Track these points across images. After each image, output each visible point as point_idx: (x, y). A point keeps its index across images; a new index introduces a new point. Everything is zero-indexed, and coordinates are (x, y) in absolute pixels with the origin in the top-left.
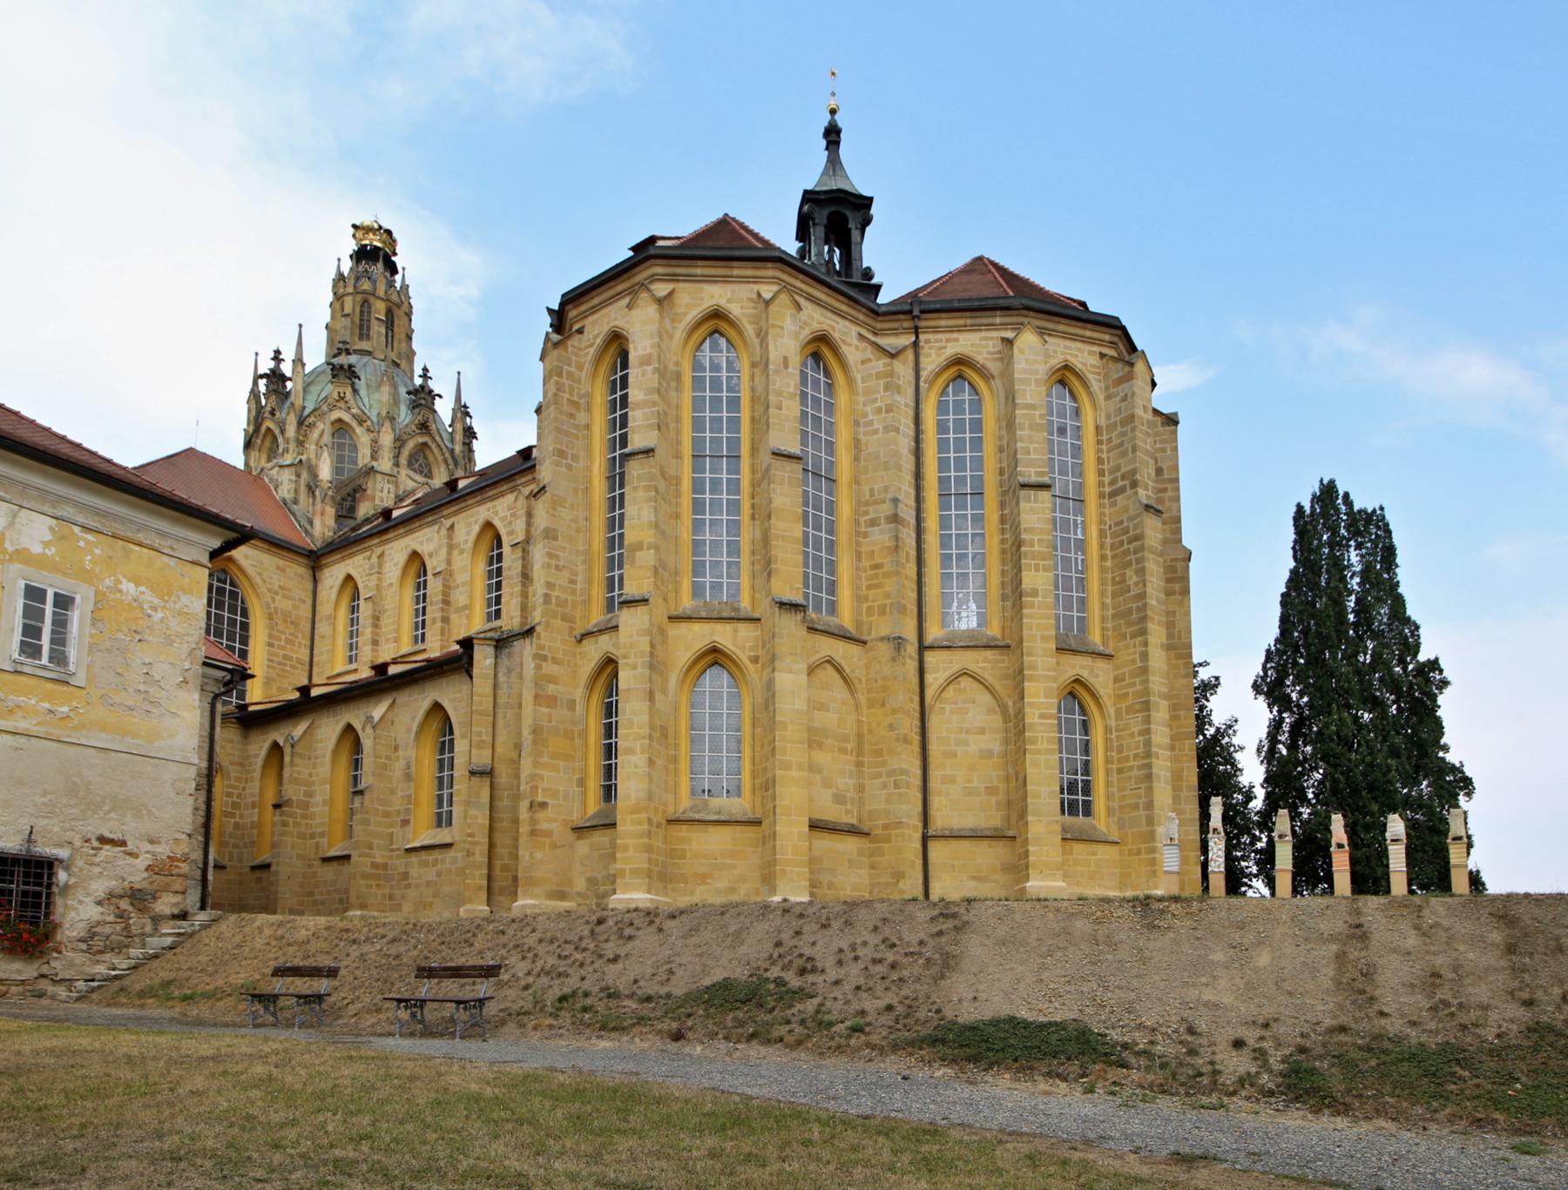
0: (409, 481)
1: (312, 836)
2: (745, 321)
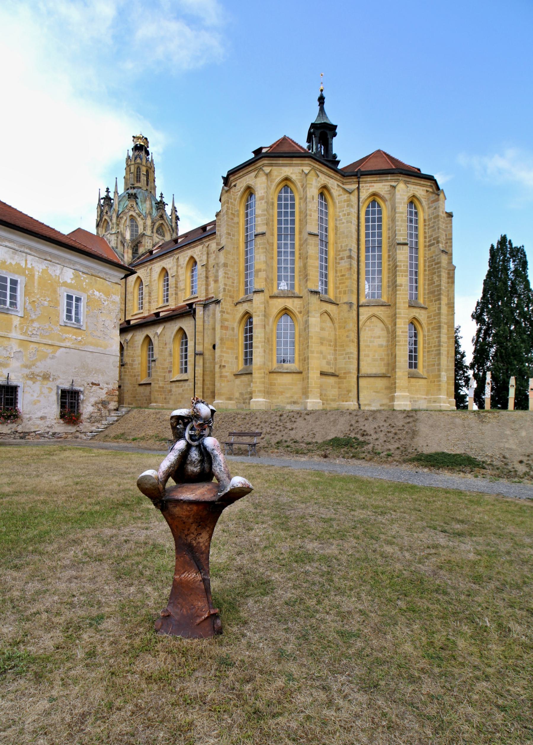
0: (157, 238)
1: (135, 376)
2: (297, 181)
